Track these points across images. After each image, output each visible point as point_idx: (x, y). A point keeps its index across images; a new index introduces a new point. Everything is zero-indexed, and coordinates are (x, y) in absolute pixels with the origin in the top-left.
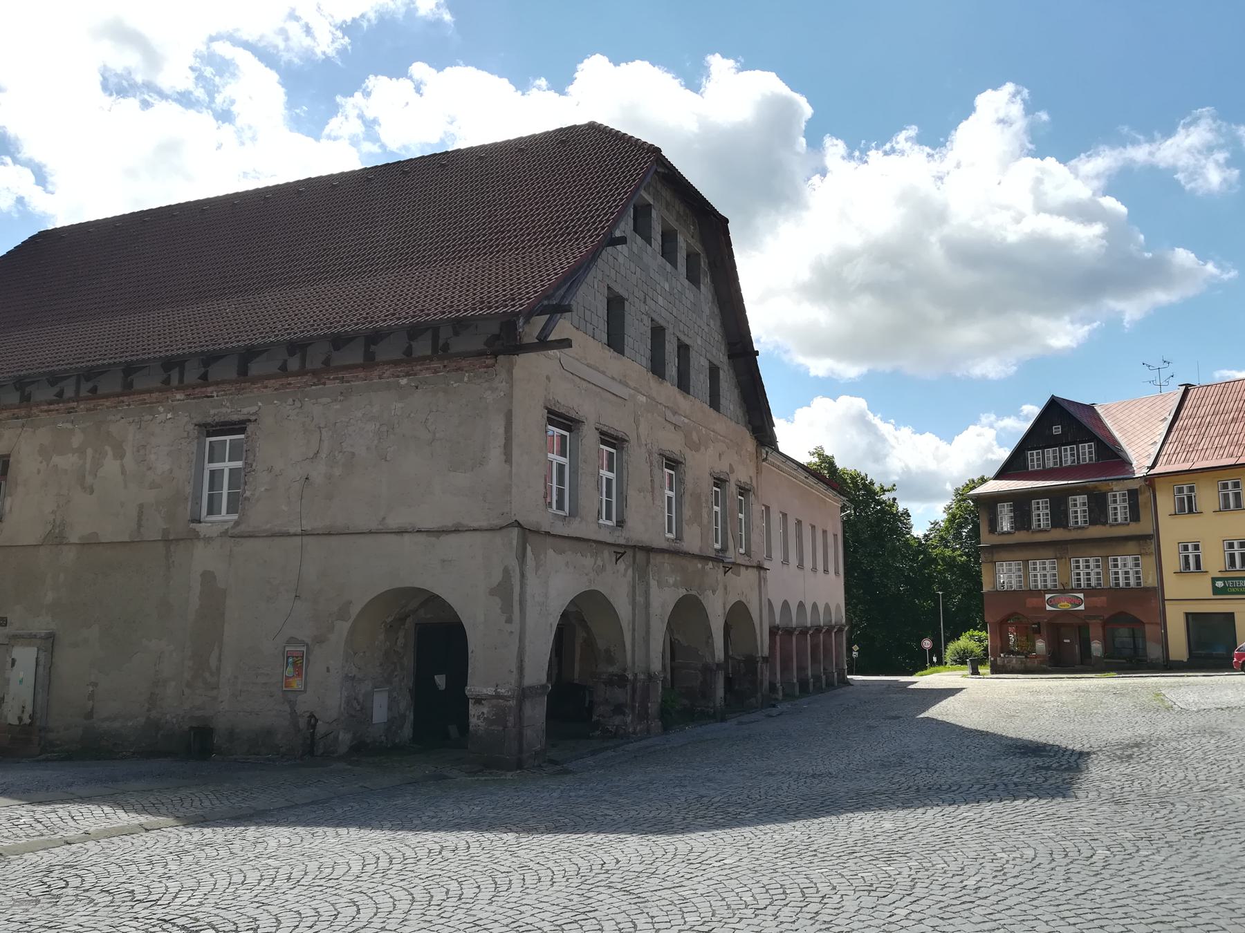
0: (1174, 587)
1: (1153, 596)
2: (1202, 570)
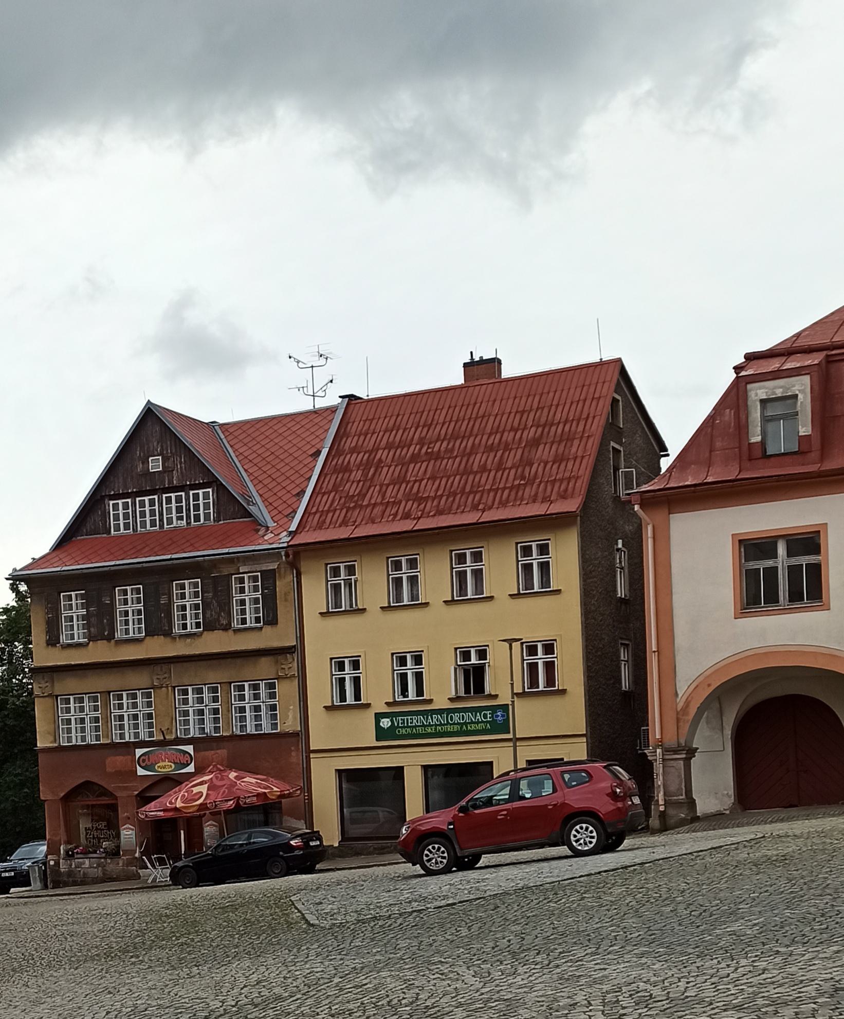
2: (487, 692)
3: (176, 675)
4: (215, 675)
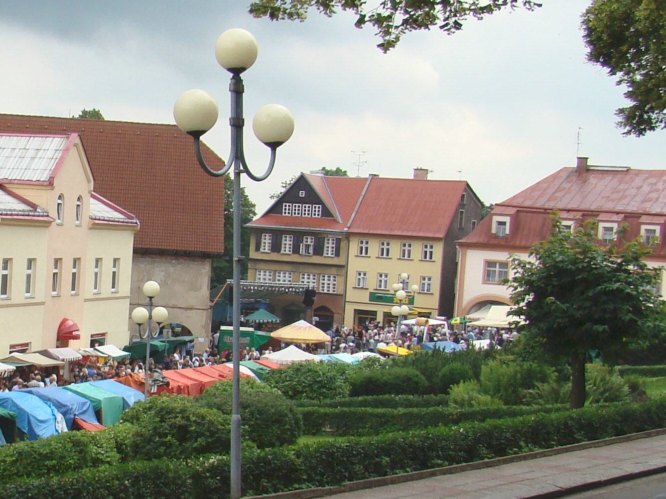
0: (351, 295)
1: (340, 298)
3: (301, 269)
4: (315, 271)
